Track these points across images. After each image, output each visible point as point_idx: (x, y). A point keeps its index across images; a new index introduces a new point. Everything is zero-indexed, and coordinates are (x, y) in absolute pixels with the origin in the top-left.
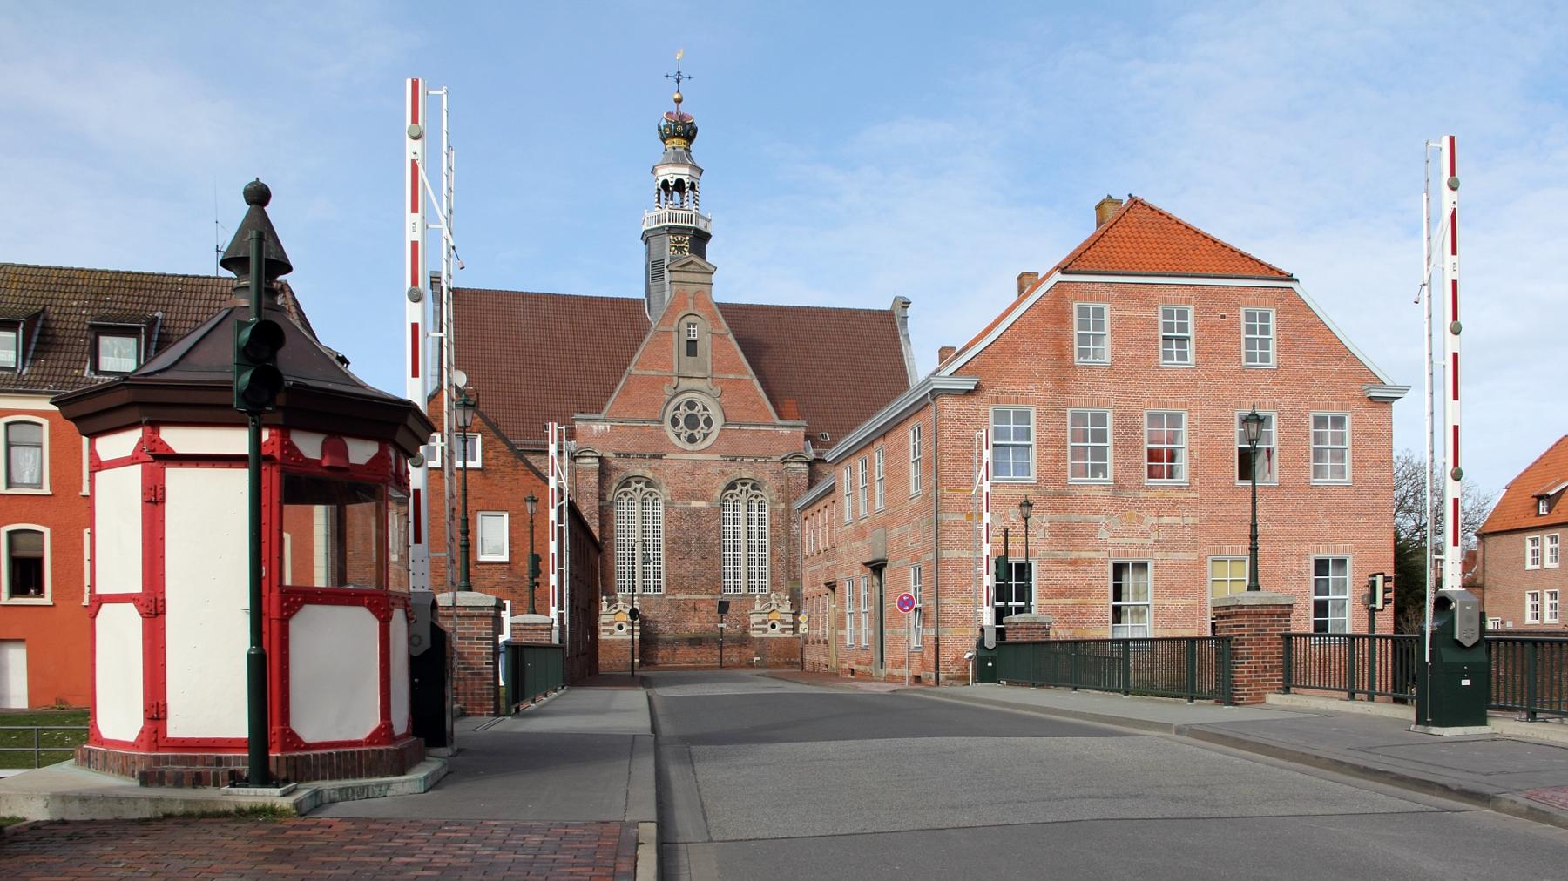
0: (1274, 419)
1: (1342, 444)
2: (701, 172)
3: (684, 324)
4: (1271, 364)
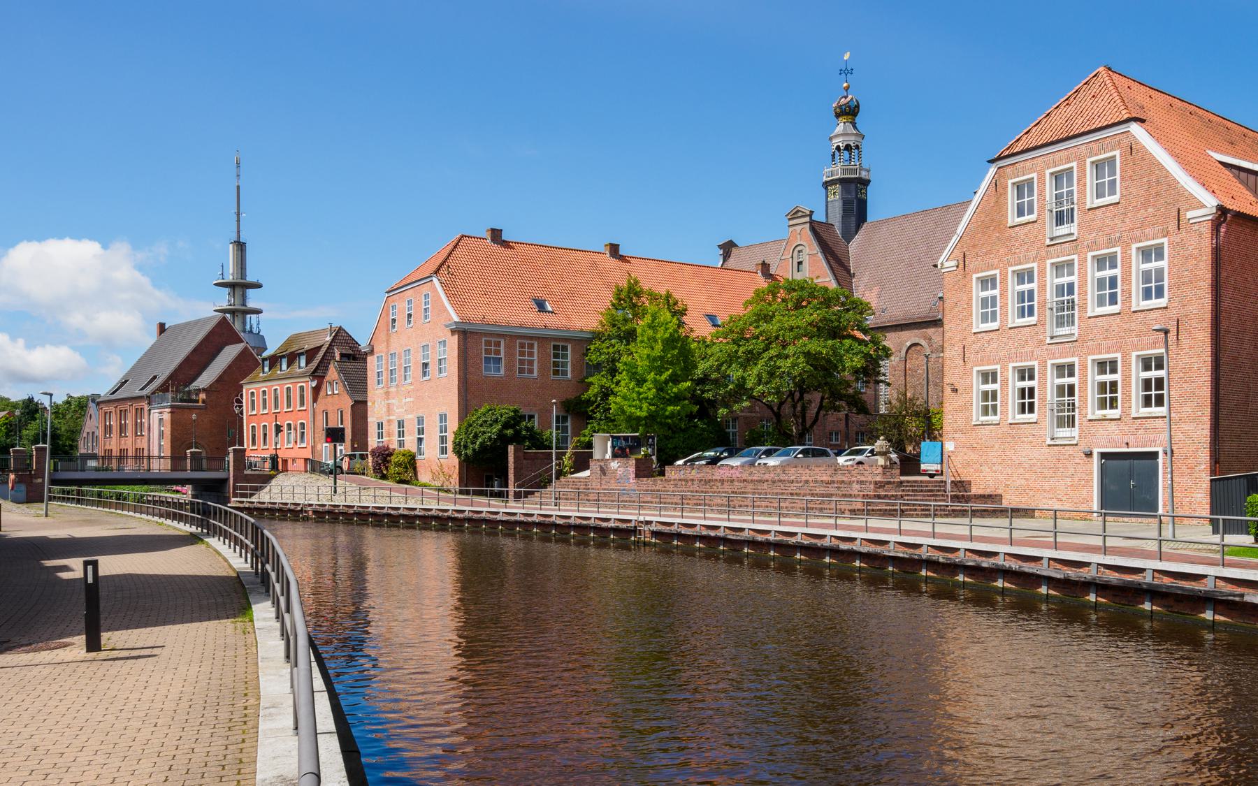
0: (536, 417)
1: (1116, 361)
3: (796, 252)
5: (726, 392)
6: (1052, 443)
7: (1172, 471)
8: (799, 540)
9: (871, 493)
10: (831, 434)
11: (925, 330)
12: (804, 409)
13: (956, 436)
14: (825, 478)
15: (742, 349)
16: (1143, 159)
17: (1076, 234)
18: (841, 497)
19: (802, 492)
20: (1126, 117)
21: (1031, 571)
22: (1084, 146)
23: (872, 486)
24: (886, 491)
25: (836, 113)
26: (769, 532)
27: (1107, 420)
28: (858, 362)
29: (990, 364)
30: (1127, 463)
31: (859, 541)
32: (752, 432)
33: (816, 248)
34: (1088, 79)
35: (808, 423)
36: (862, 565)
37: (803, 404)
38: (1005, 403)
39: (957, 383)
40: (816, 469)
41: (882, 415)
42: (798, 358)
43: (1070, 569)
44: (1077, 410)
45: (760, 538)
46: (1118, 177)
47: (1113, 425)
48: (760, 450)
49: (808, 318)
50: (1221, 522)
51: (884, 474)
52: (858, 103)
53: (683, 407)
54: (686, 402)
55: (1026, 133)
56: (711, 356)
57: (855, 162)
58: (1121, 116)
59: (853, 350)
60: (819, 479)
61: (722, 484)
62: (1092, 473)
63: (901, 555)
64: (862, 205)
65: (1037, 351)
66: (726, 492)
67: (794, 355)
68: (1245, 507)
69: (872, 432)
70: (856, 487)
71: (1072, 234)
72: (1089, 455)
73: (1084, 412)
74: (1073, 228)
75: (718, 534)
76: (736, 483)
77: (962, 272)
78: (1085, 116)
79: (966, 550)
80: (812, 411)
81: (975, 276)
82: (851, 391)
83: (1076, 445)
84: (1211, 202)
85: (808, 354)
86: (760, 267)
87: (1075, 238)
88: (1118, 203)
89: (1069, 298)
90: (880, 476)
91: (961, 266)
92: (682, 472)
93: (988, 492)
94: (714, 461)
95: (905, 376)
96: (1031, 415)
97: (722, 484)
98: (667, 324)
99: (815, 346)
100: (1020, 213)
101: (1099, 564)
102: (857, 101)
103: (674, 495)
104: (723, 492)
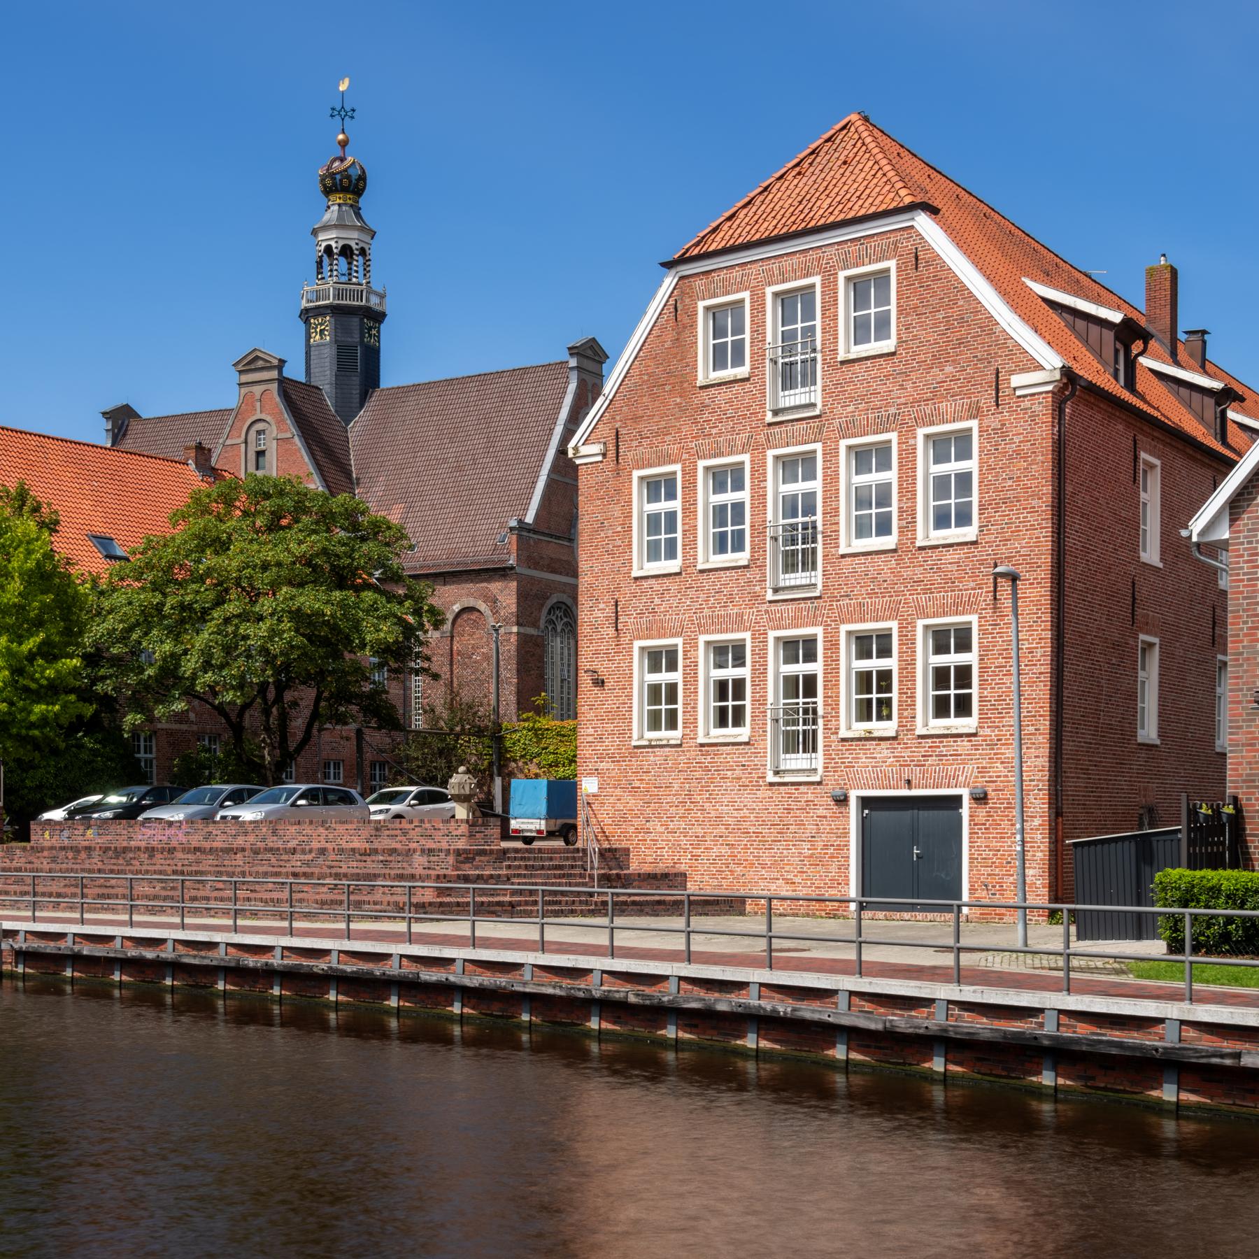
1: (890, 636)
2: (373, 235)
4: (782, 576)
5: (140, 682)
6: (777, 779)
7: (1023, 829)
8: (334, 964)
9: (449, 872)
10: (327, 765)
11: (485, 584)
12: (284, 718)
13: (602, 766)
14: (356, 844)
15: (171, 601)
16: (936, 279)
17: (819, 406)
18: (394, 879)
19: (317, 870)
20: (908, 200)
21: (816, 1017)
22: (833, 250)
23: (451, 859)
24: (477, 868)
25: (325, 186)
26: (270, 949)
27: (874, 739)
28: (388, 632)
29: (664, 636)
30: (906, 815)
31: (459, 965)
32: (186, 759)
33: (291, 430)
34: (832, 132)
35: (292, 746)
36: (466, 1010)
37: (284, 708)
38: (691, 707)
39: (603, 668)
40: (338, 826)
41: (418, 733)
42: (280, 620)
43: (891, 1011)
44: (820, 721)
45: (251, 961)
46: (893, 307)
47: (883, 751)
48: (222, 791)
49: (298, 550)
50: (1187, 920)
51: (471, 836)
52: (364, 172)
53: (64, 707)
54: (72, 697)
55: (729, 219)
56: (109, 613)
57: (358, 278)
58: (897, 198)
59: (377, 610)
60: (345, 845)
61: (151, 857)
62: (846, 834)
63: (550, 991)
64: (372, 357)
65: (749, 614)
66: (160, 872)
67: (272, 615)
68: (1152, 890)
69: (400, 763)
70: (419, 861)
71: (813, 405)
72: (842, 801)
73: (832, 725)
74: (814, 395)
75: (163, 955)
76: (180, 855)
77: (612, 465)
78: (833, 195)
79: (681, 978)
80: (298, 724)
81: (636, 474)
82: (367, 688)
83: (819, 783)
84: (1052, 360)
85: (297, 616)
86: (193, 454)
87: (817, 412)
88: (893, 354)
89: (806, 519)
90: (463, 840)
91: (611, 454)
92: (66, 833)
93: (661, 868)
94: (129, 813)
95: (451, 664)
96: (737, 730)
97: (151, 857)
98: (28, 543)
99: (311, 600)
100: (719, 363)
101: (949, 1002)
102: (362, 168)
103: (53, 879)
104: (155, 872)
